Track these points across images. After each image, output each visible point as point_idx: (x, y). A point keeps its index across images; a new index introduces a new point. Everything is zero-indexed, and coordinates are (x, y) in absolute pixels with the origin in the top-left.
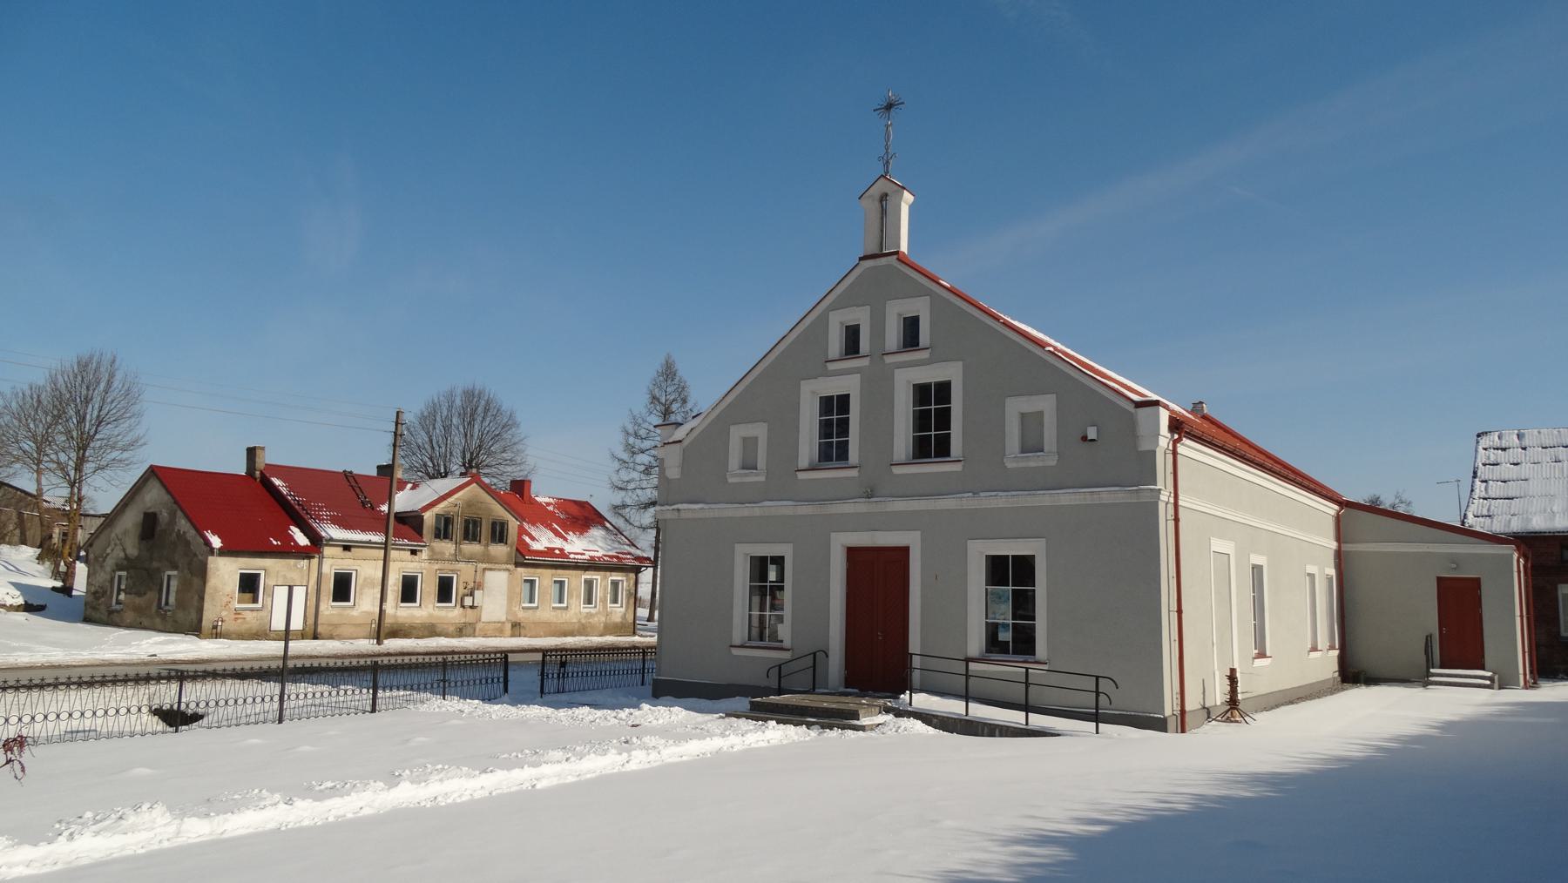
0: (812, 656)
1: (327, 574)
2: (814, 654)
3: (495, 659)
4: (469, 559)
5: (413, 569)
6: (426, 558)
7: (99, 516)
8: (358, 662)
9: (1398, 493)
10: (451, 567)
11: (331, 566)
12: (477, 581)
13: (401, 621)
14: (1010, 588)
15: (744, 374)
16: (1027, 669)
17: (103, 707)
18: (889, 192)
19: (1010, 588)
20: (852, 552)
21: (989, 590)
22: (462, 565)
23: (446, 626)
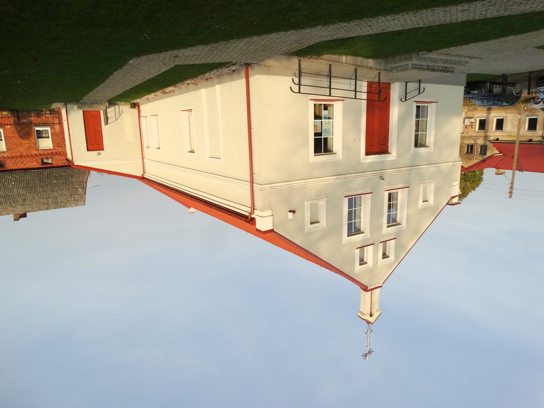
0: (407, 99)
1: (540, 129)
2: (406, 100)
3: (478, 97)
4: (470, 137)
5: (497, 133)
6: (491, 137)
7: (118, 118)
8: (536, 94)
9: (103, 176)
10: (479, 134)
11: (538, 133)
12: (467, 129)
13: (504, 111)
14: (323, 137)
15: (390, 276)
16: (330, 95)
17: (497, 89)
18: (173, 93)
19: (323, 137)
20: (368, 153)
21: (332, 135)
22: (474, 135)
23: (482, 109)
